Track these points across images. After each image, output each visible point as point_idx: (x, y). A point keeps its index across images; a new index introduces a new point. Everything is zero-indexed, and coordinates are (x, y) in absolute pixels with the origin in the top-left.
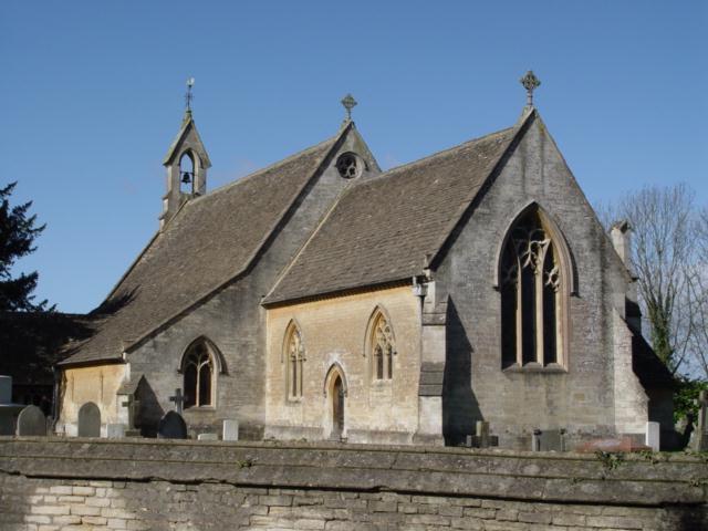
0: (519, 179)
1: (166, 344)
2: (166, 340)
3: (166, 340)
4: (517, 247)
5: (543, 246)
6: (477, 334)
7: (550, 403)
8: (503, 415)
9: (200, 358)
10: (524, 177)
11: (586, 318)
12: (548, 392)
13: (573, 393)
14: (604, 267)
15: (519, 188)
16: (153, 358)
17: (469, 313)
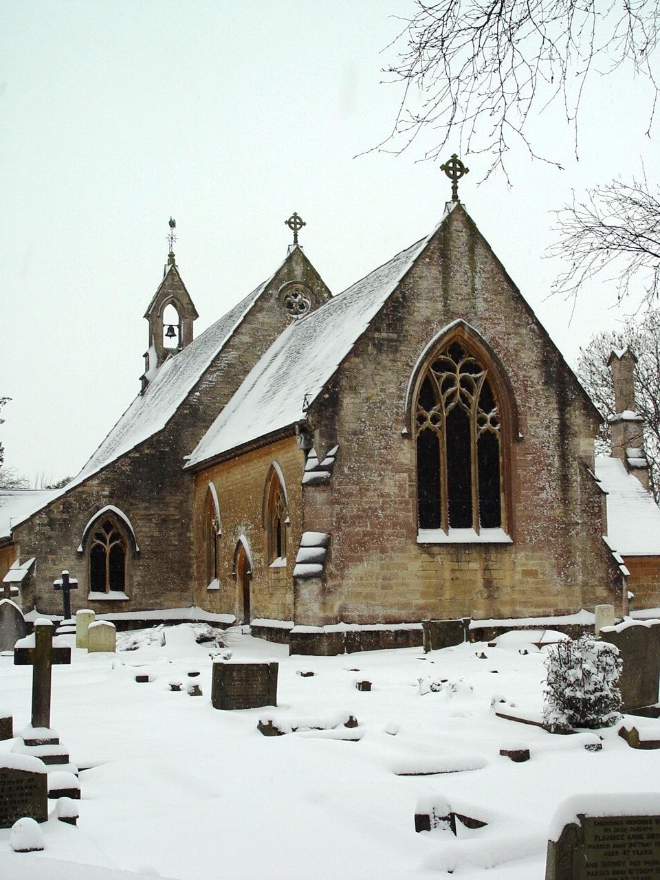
0: (439, 293)
1: (65, 520)
2: (65, 516)
3: (65, 516)
5: (477, 380)
6: (382, 496)
7: (488, 583)
8: (421, 602)
9: (108, 538)
10: (445, 290)
11: (539, 471)
12: (486, 569)
13: (519, 569)
14: (563, 405)
15: (440, 306)
16: (50, 538)
17: (368, 469)
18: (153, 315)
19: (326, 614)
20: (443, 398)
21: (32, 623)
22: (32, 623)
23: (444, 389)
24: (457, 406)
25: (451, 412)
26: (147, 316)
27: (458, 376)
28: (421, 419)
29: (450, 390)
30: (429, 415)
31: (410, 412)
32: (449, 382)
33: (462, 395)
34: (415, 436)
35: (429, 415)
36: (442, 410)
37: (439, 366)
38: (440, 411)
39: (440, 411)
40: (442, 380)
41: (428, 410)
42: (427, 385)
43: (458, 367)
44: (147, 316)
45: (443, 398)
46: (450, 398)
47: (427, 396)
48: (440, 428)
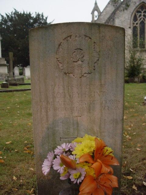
4: (138, 16)
18: (93, 13)
19: (26, 38)
20: (139, 19)
21: (44, 162)
22: (44, 162)
23: (139, 17)
24: (142, 21)
25: (141, 22)
26: (91, 14)
27: (142, 14)
28: (133, 24)
29: (140, 17)
30: (135, 23)
31: (70, 96)
32: (140, 15)
33: (143, 18)
34: (132, 28)
35: (135, 23)
36: (139, 22)
37: (138, 12)
38: (138, 22)
39: (138, 22)
40: (138, 15)
41: (135, 22)
42: (135, 16)
43: (142, 12)
44: (91, 14)
45: (139, 19)
46: (140, 19)
47: (135, 19)
48: (138, 26)
